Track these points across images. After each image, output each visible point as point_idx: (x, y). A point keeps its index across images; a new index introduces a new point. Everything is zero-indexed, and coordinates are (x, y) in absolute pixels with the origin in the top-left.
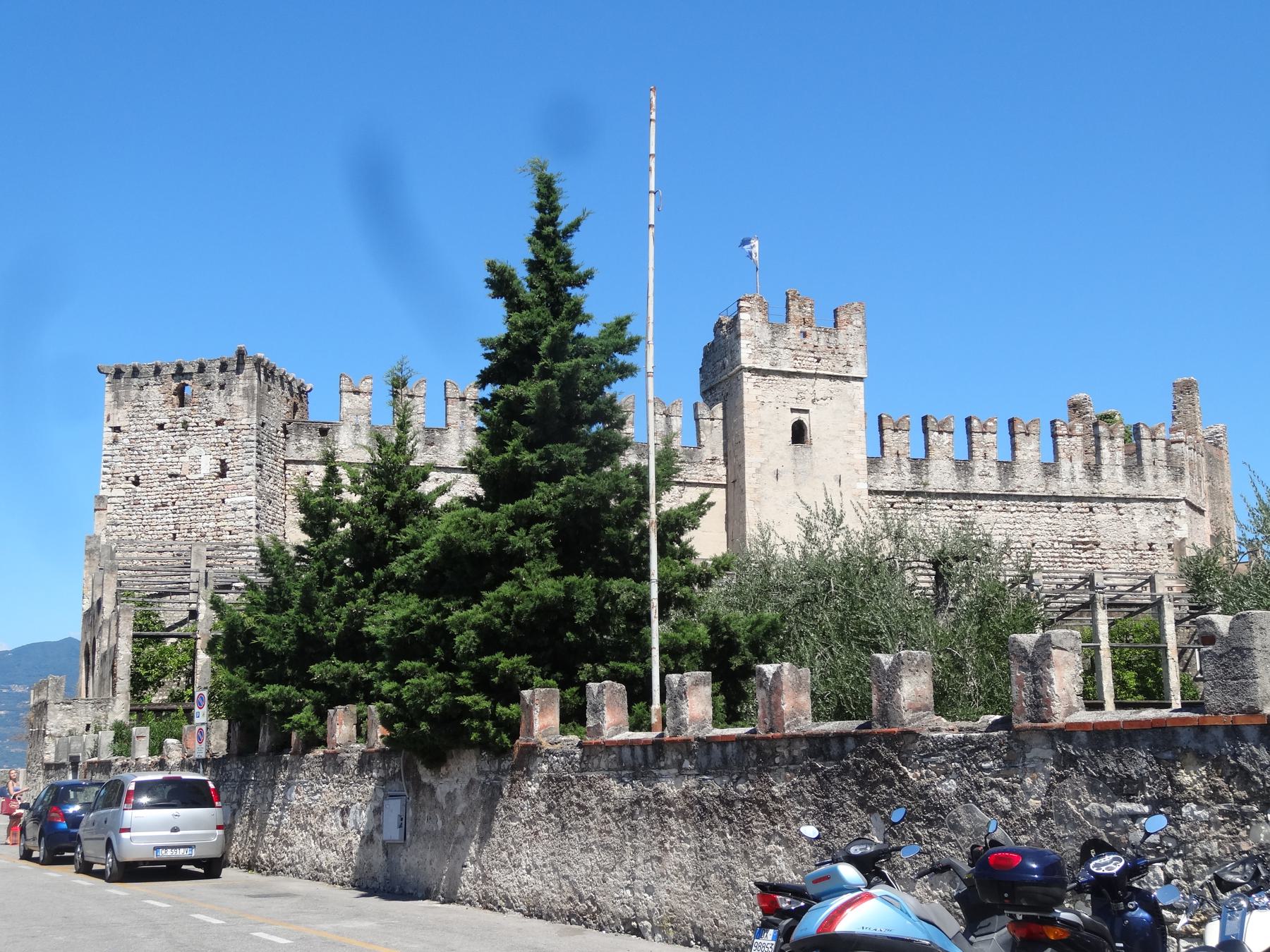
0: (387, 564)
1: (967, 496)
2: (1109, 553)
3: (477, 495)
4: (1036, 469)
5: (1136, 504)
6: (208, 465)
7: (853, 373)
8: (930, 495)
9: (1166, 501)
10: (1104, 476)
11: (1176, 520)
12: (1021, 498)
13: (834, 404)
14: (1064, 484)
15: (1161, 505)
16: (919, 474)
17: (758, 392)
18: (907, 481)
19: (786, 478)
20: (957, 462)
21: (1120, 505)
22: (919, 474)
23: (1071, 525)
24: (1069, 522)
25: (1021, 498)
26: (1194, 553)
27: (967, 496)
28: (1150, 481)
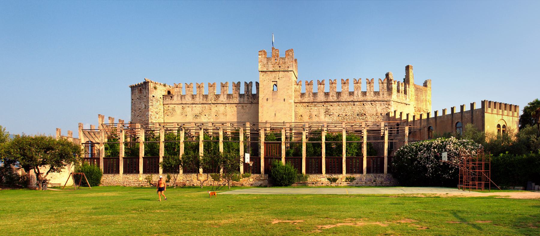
0: (199, 160)
1: (327, 102)
2: (369, 117)
3: (63, 168)
4: (347, 93)
5: (377, 102)
6: (143, 106)
7: (289, 70)
8: (318, 102)
9: (386, 101)
10: (367, 94)
11: (389, 107)
12: (343, 102)
13: (284, 79)
14: (355, 97)
15: (385, 103)
16: (315, 97)
17: (264, 77)
18: (311, 99)
19: (270, 101)
20: (325, 93)
21: (372, 103)
22: (315, 97)
23: (357, 109)
24: (357, 108)
25: (343, 102)
26: (109, 122)
27: (327, 102)
28: (381, 96)
